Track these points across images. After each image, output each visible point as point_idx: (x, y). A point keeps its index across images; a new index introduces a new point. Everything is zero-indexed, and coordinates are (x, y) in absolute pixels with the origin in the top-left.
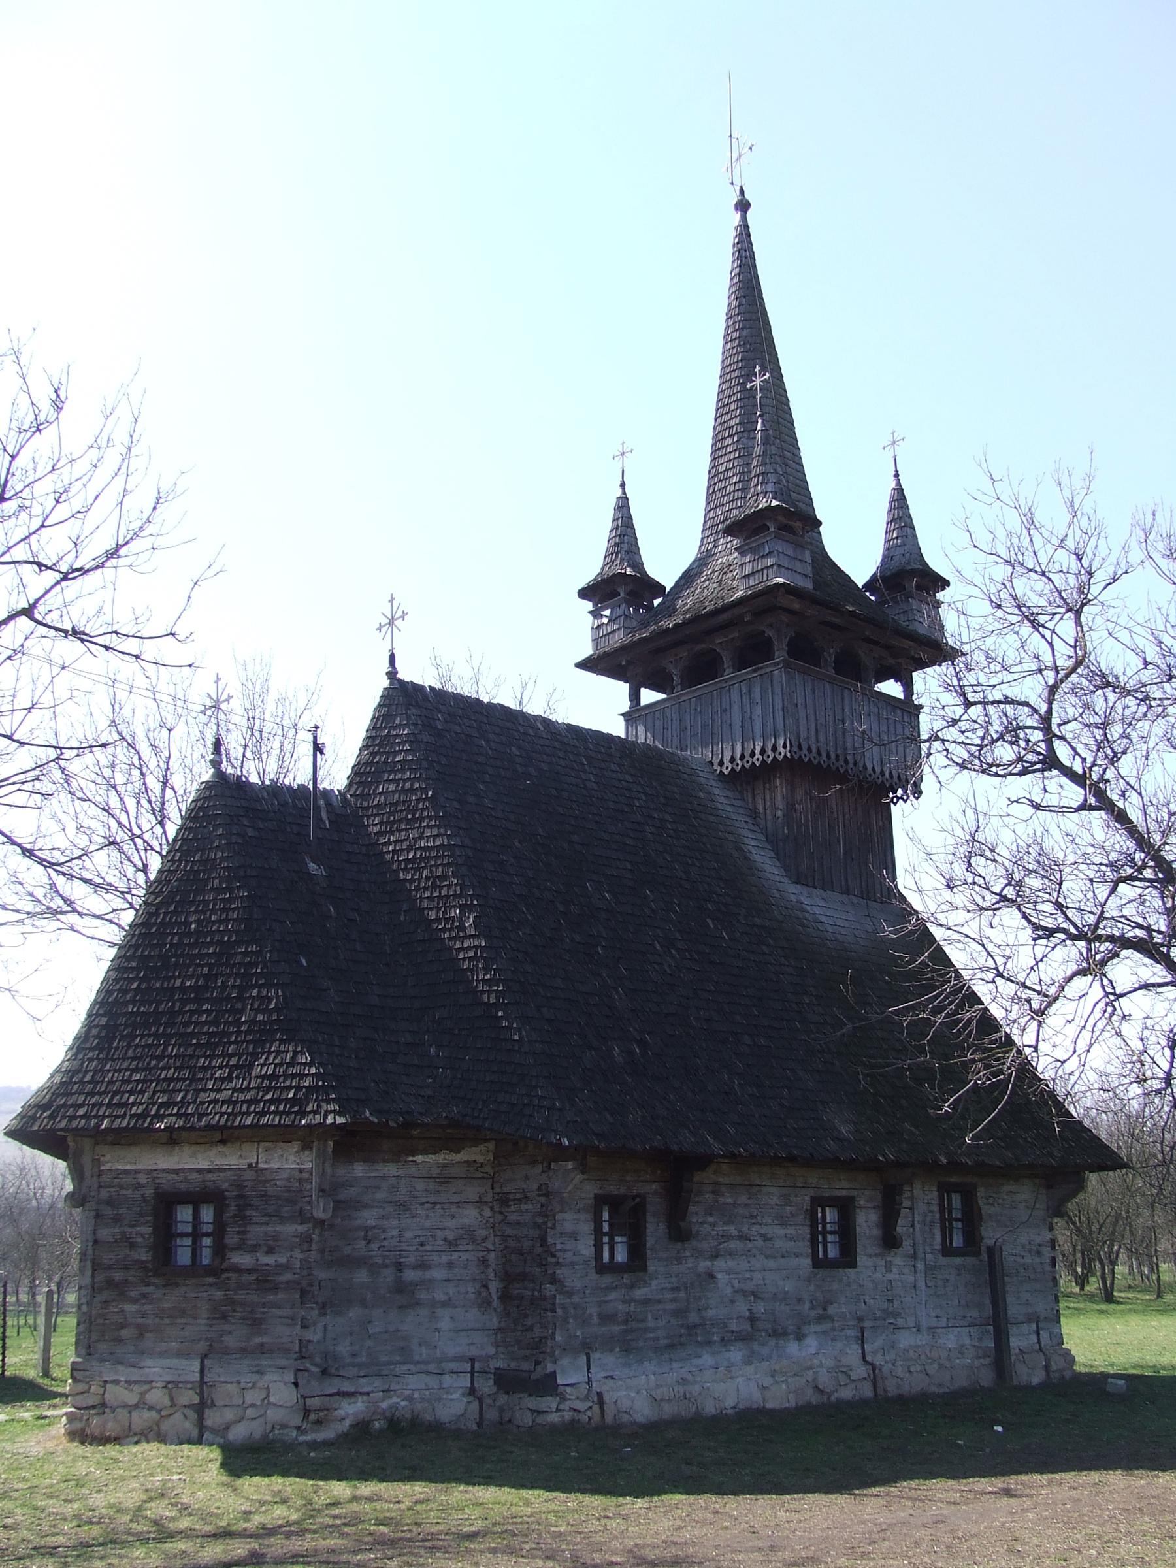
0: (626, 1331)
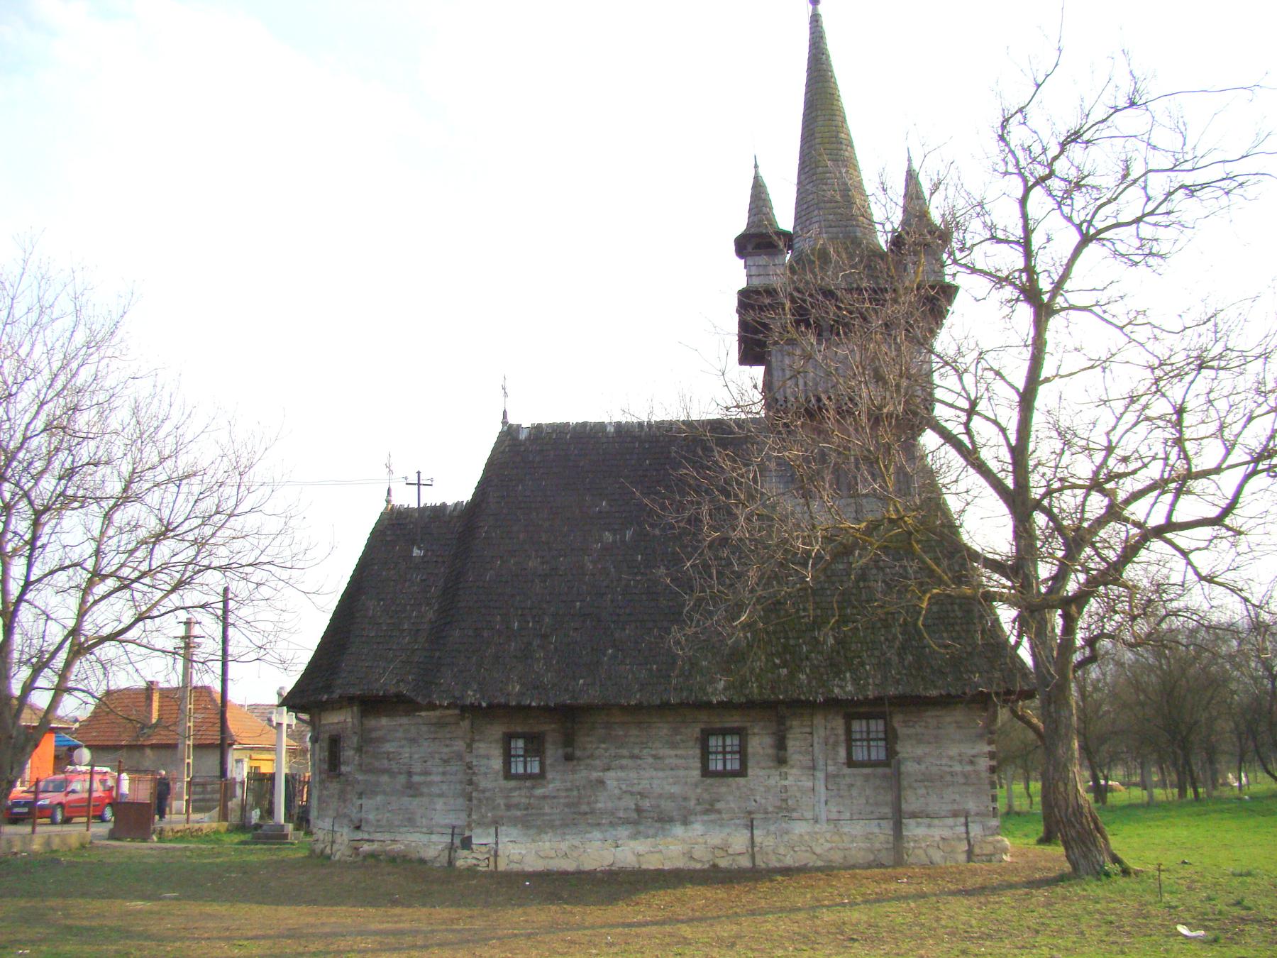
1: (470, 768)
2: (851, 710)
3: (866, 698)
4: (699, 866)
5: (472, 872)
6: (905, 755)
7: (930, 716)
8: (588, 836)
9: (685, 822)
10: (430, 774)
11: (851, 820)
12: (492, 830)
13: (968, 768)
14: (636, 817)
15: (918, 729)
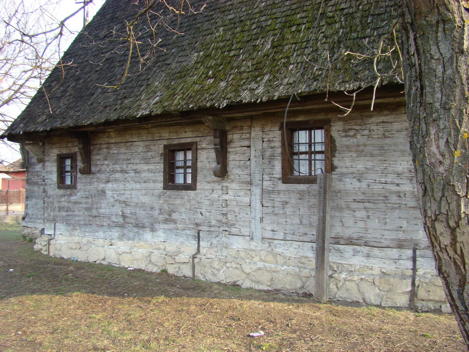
12: (53, 225)
15: (360, 139)
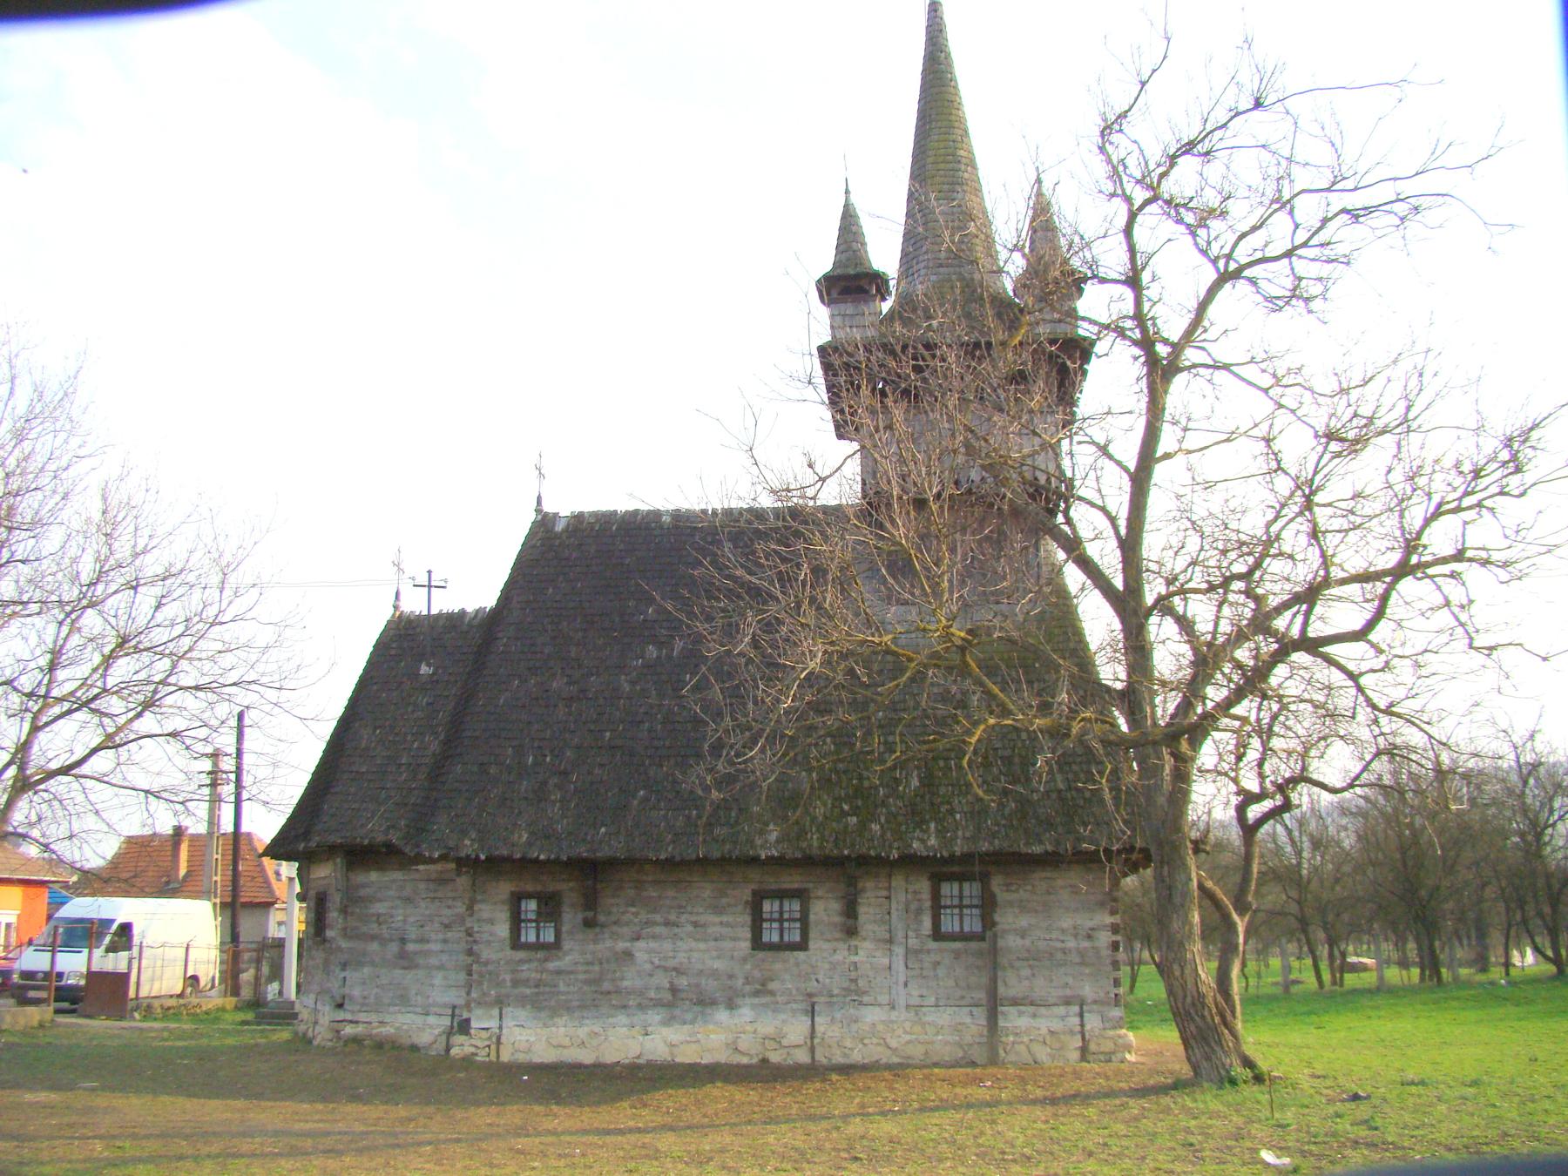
0: (537, 994)
1: (470, 935)
2: (940, 869)
3: (952, 856)
4: (745, 1060)
5: (468, 1062)
6: (1007, 927)
7: (1040, 879)
8: (611, 1020)
9: (731, 1006)
10: (428, 942)
11: (937, 1006)
12: (496, 1012)
13: (1086, 944)
14: (671, 998)
15: (1022, 894)
